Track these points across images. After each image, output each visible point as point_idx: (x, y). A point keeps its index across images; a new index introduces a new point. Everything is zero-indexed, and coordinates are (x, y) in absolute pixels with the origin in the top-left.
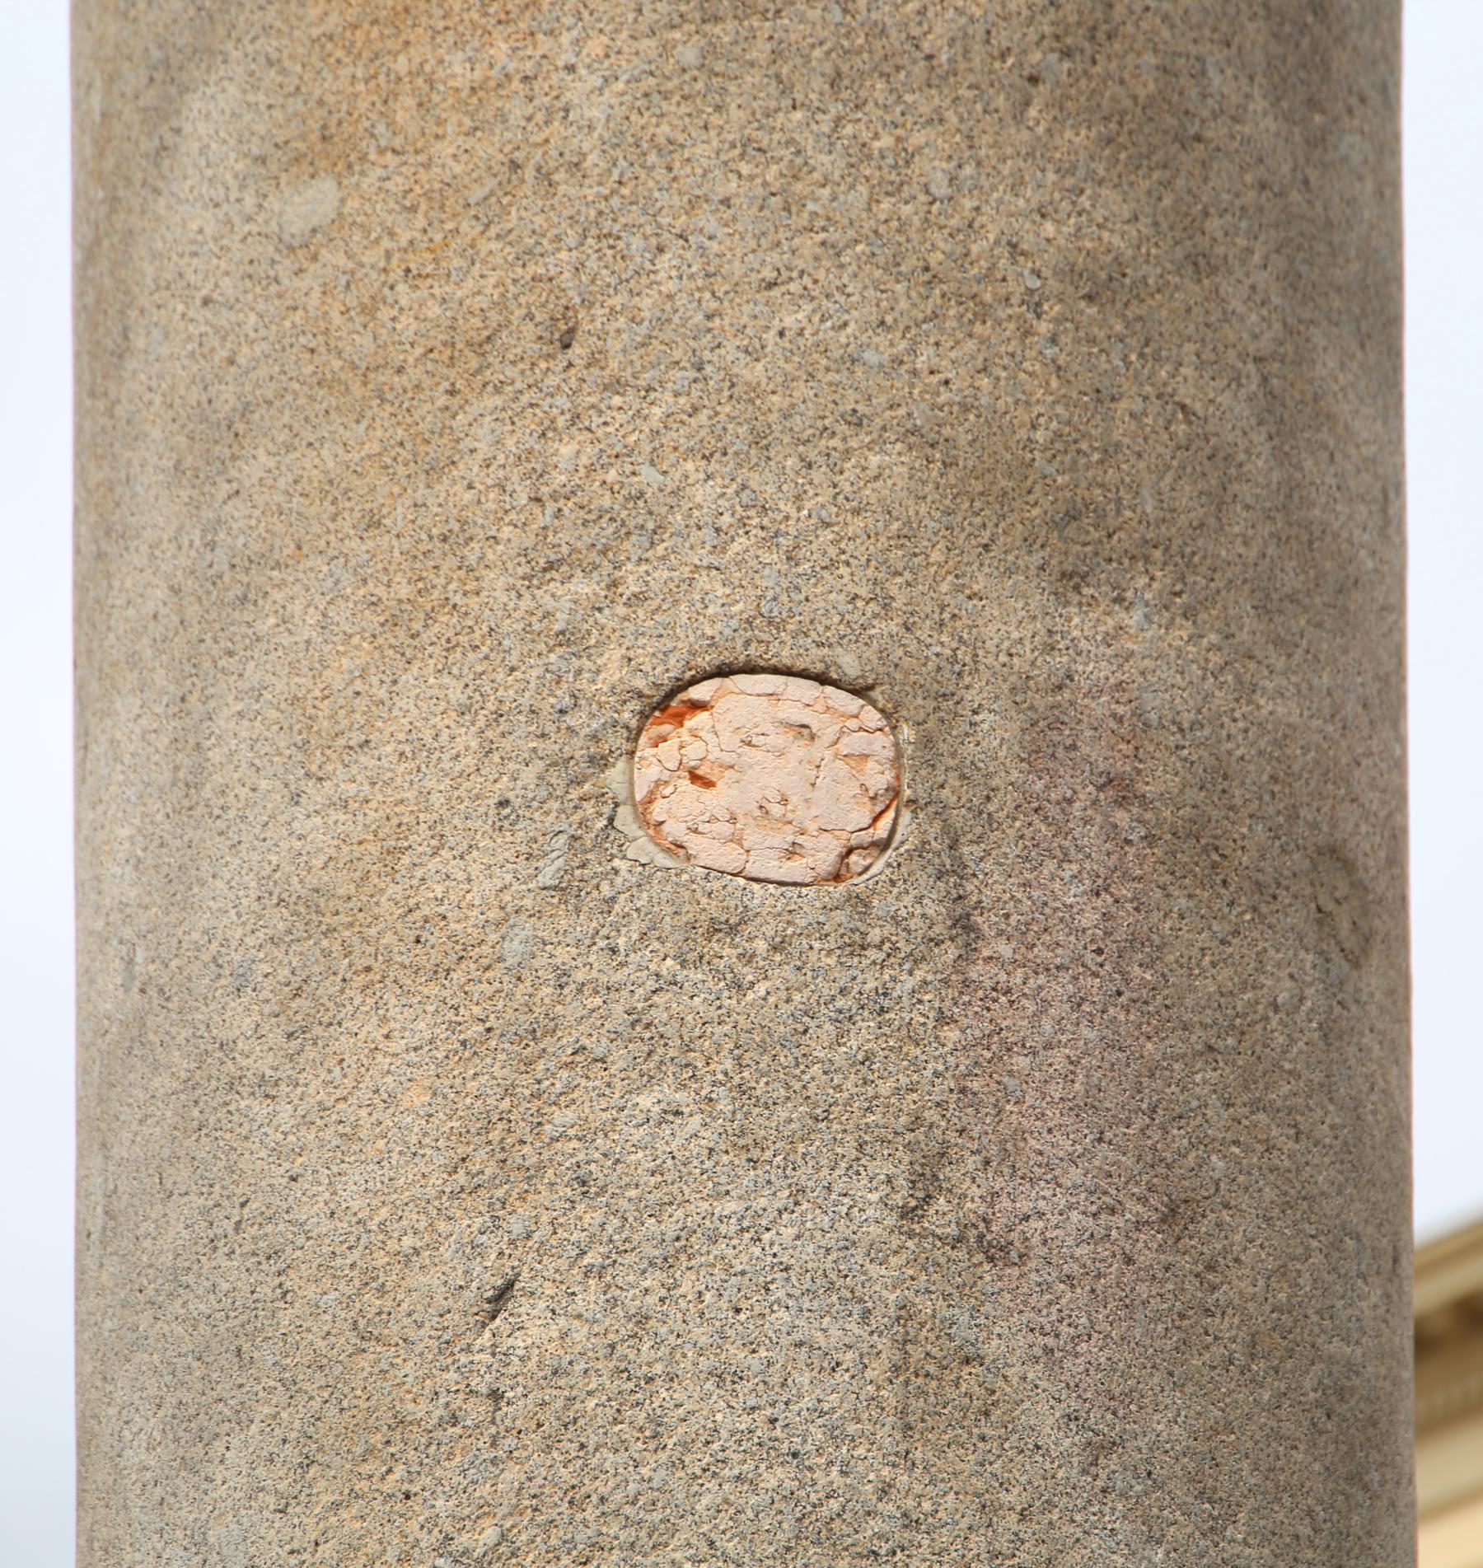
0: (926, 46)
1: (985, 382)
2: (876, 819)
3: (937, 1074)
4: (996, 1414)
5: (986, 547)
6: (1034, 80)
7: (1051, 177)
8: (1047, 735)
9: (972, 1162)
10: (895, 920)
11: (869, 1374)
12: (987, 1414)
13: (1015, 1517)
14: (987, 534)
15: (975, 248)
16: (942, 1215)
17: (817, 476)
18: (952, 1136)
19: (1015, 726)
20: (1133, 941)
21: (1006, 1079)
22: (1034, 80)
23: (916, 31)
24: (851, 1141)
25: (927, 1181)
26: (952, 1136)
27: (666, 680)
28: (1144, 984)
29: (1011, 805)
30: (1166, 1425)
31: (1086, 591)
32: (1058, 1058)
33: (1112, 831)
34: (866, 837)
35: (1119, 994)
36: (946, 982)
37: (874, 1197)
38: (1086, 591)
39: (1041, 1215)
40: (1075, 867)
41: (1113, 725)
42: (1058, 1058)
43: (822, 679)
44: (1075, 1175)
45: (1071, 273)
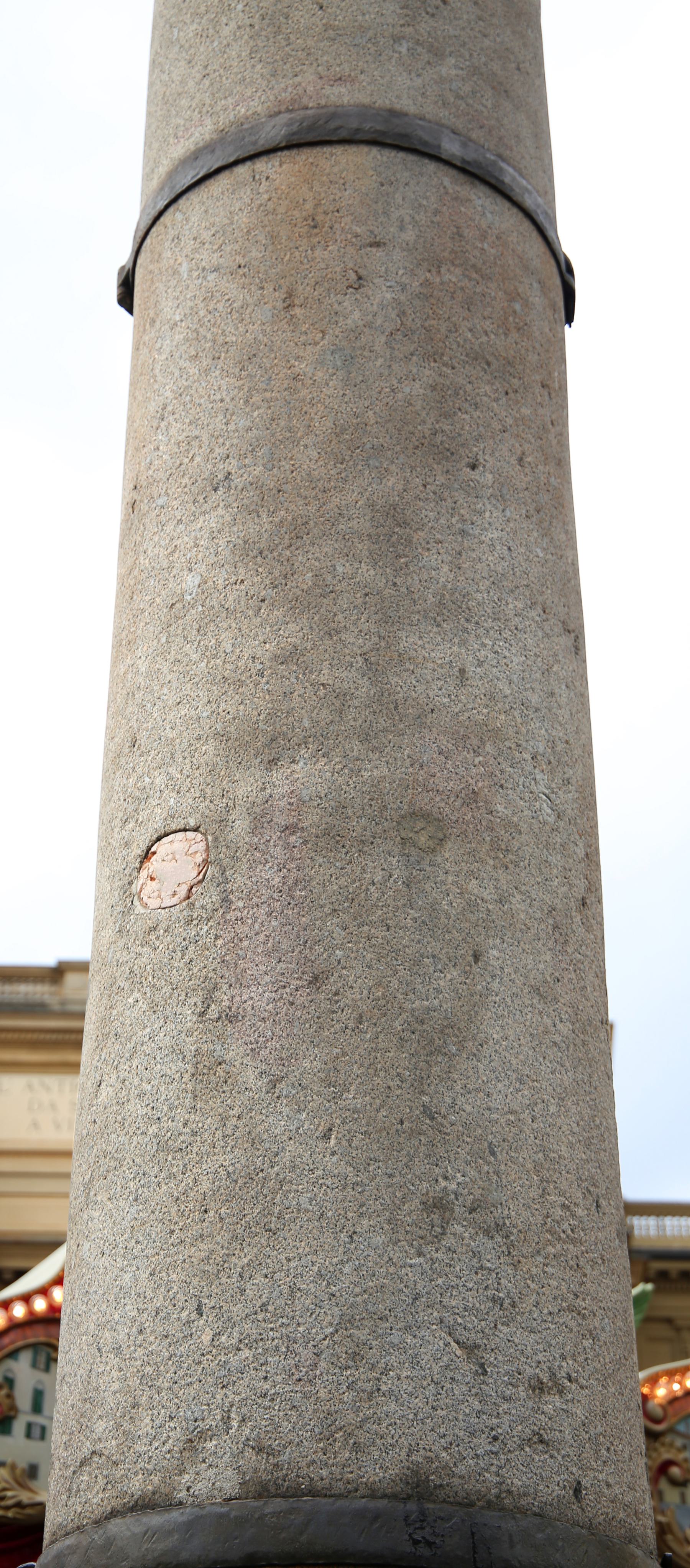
0: (226, 606)
1: (242, 707)
2: (199, 873)
3: (214, 959)
4: (229, 1081)
5: (240, 763)
6: (263, 601)
7: (268, 629)
8: (260, 820)
9: (225, 987)
10: (202, 907)
11: (184, 1080)
12: (226, 1082)
13: (235, 1119)
14: (240, 759)
15: (240, 664)
16: (213, 1011)
17: (187, 761)
18: (219, 980)
19: (247, 822)
20: (296, 882)
21: (239, 952)
22: (263, 601)
23: (223, 603)
24: (184, 994)
25: (208, 1001)
26: (219, 980)
27: (145, 848)
28: (301, 896)
29: (245, 850)
30: (310, 1063)
31: (279, 764)
32: (262, 938)
33: (288, 847)
34: (196, 881)
35: (289, 904)
36: (219, 924)
37: (189, 1012)
38: (279, 764)
39: (252, 998)
40: (270, 864)
41: (289, 807)
42: (262, 938)
43: (185, 830)
44: (267, 978)
45: (276, 657)
